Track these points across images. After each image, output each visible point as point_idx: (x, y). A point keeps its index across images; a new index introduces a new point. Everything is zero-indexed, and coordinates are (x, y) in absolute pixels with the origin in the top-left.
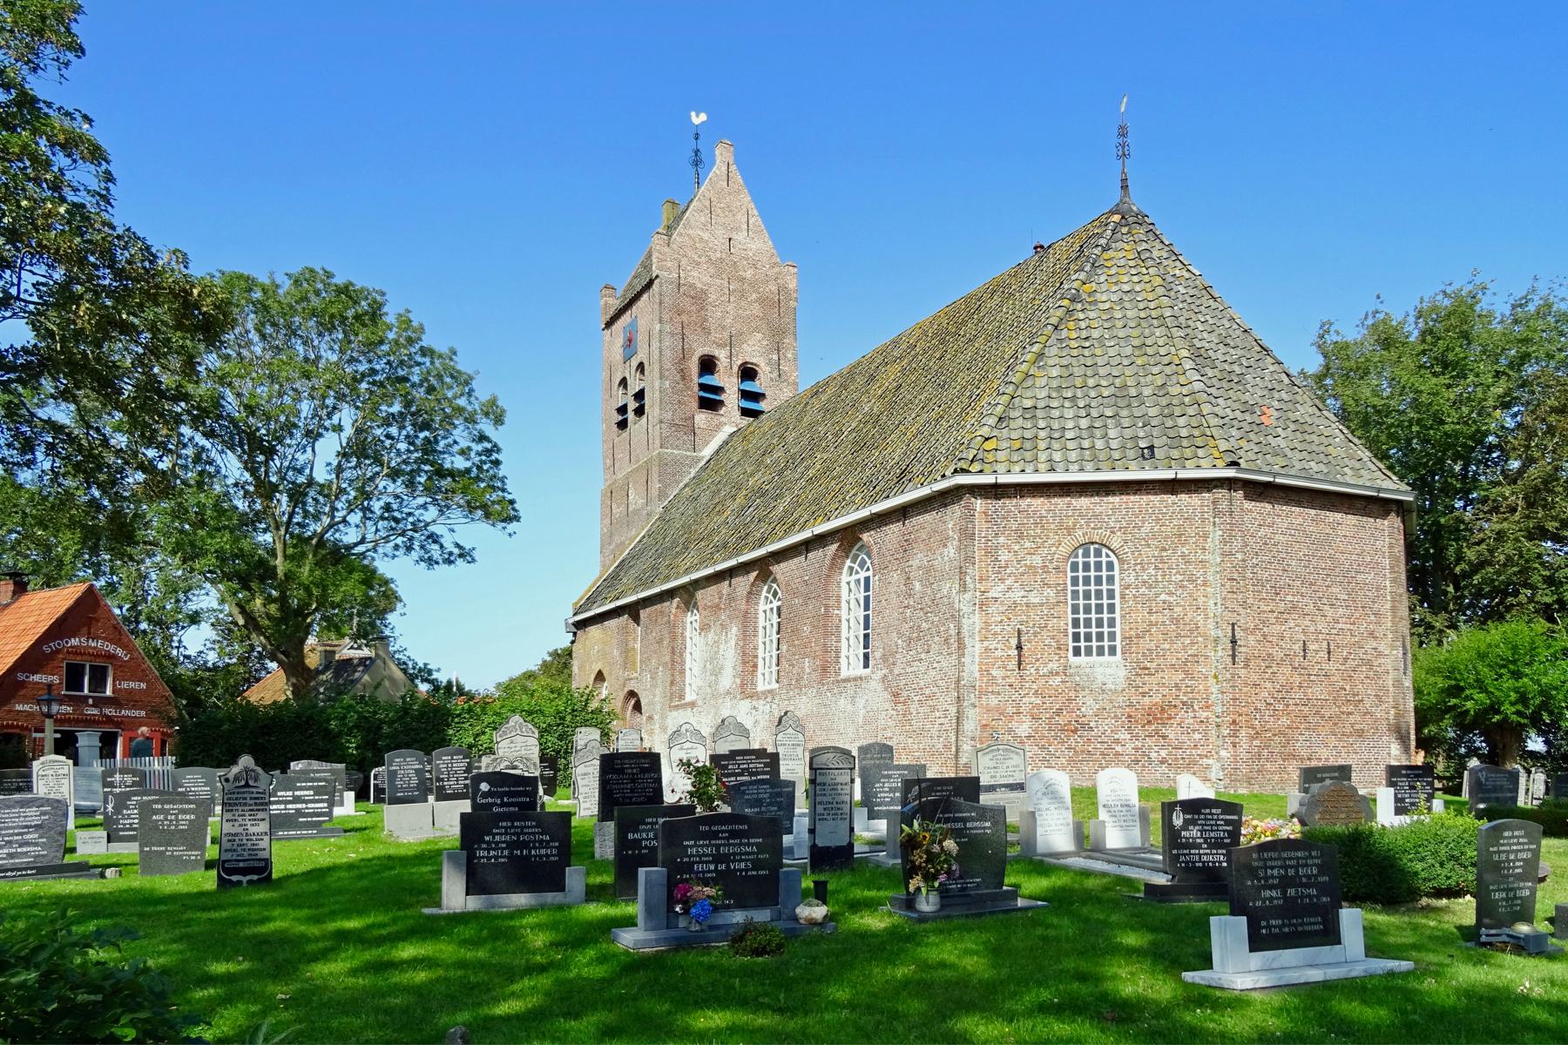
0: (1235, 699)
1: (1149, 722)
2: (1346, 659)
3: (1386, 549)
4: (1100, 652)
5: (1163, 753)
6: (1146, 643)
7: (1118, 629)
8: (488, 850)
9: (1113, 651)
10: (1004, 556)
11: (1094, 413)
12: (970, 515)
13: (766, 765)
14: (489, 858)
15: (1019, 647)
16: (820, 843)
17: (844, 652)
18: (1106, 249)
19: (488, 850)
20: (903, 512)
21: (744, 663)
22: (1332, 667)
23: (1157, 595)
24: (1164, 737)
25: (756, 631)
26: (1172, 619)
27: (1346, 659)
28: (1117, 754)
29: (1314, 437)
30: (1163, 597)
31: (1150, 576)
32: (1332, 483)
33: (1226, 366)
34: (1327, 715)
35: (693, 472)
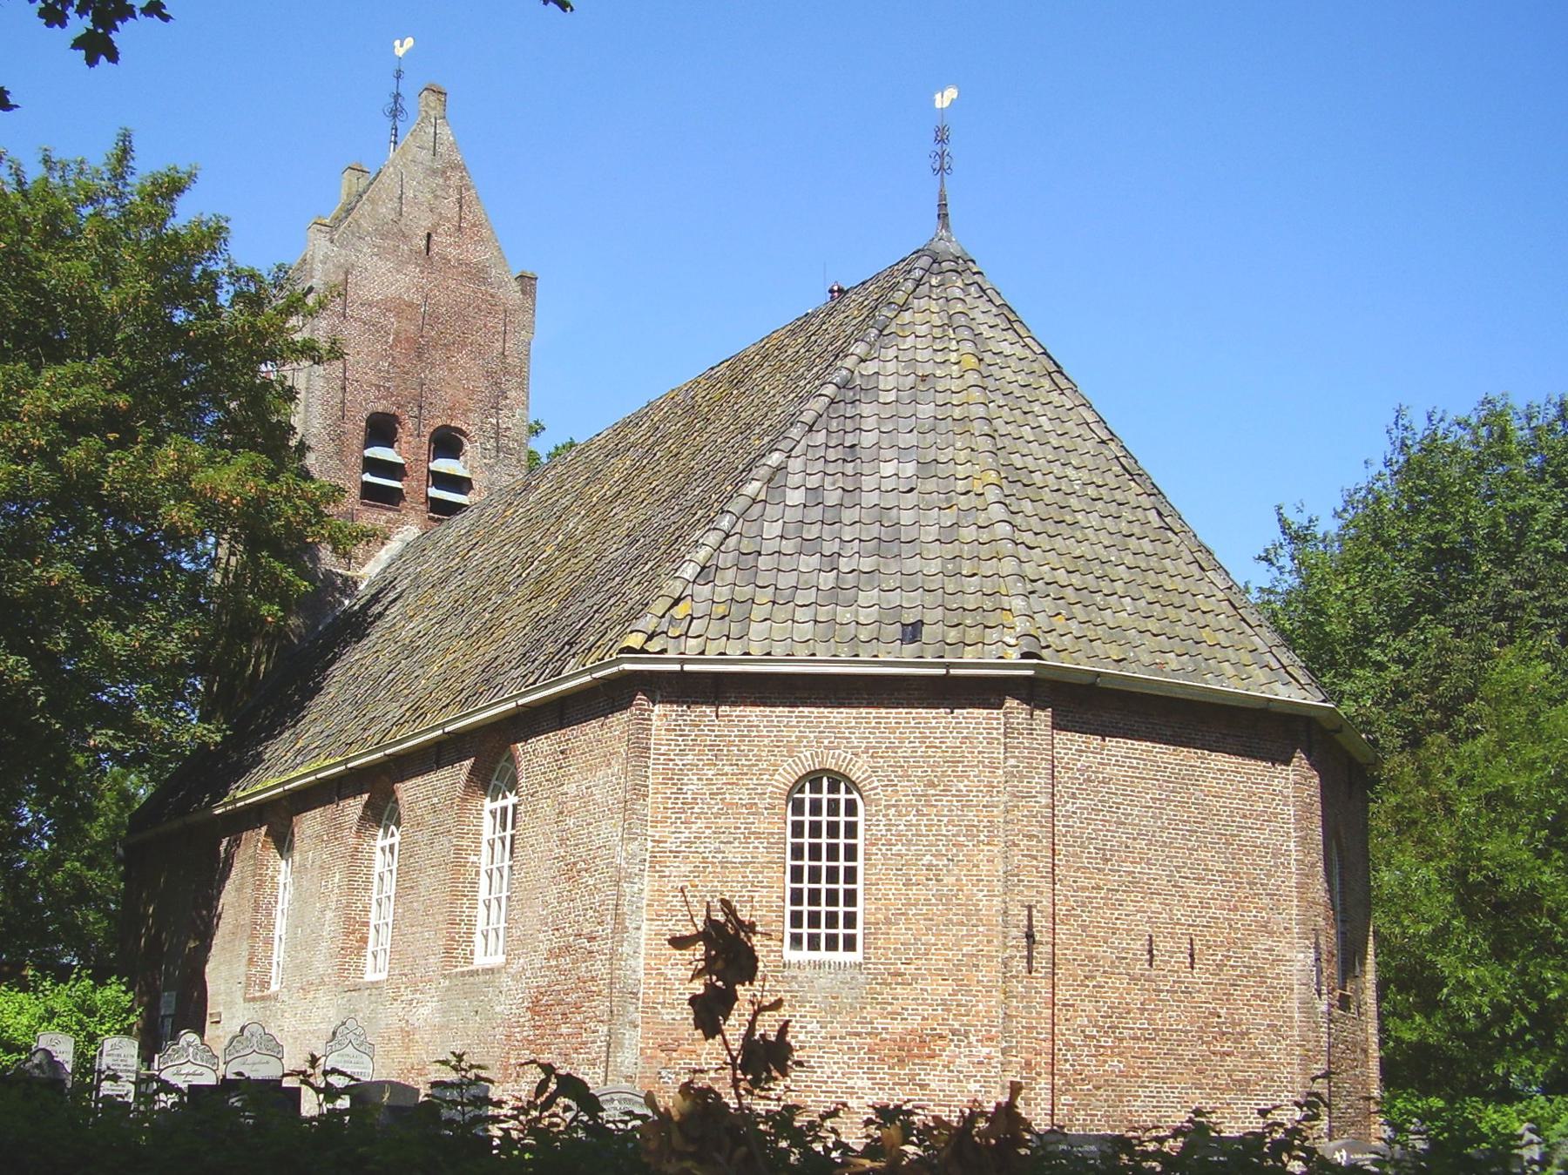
0: (1030, 1028)
1: (901, 1061)
2: (1220, 966)
3: (1289, 792)
4: (832, 944)
6: (900, 932)
7: (859, 909)
9: (850, 944)
10: (692, 785)
11: (844, 565)
12: (644, 722)
17: (481, 925)
18: (904, 307)
22: (1199, 976)
23: (919, 857)
25: (368, 881)
27: (1220, 966)
29: (1182, 614)
31: (909, 825)
33: (1058, 497)
34: (1188, 1055)
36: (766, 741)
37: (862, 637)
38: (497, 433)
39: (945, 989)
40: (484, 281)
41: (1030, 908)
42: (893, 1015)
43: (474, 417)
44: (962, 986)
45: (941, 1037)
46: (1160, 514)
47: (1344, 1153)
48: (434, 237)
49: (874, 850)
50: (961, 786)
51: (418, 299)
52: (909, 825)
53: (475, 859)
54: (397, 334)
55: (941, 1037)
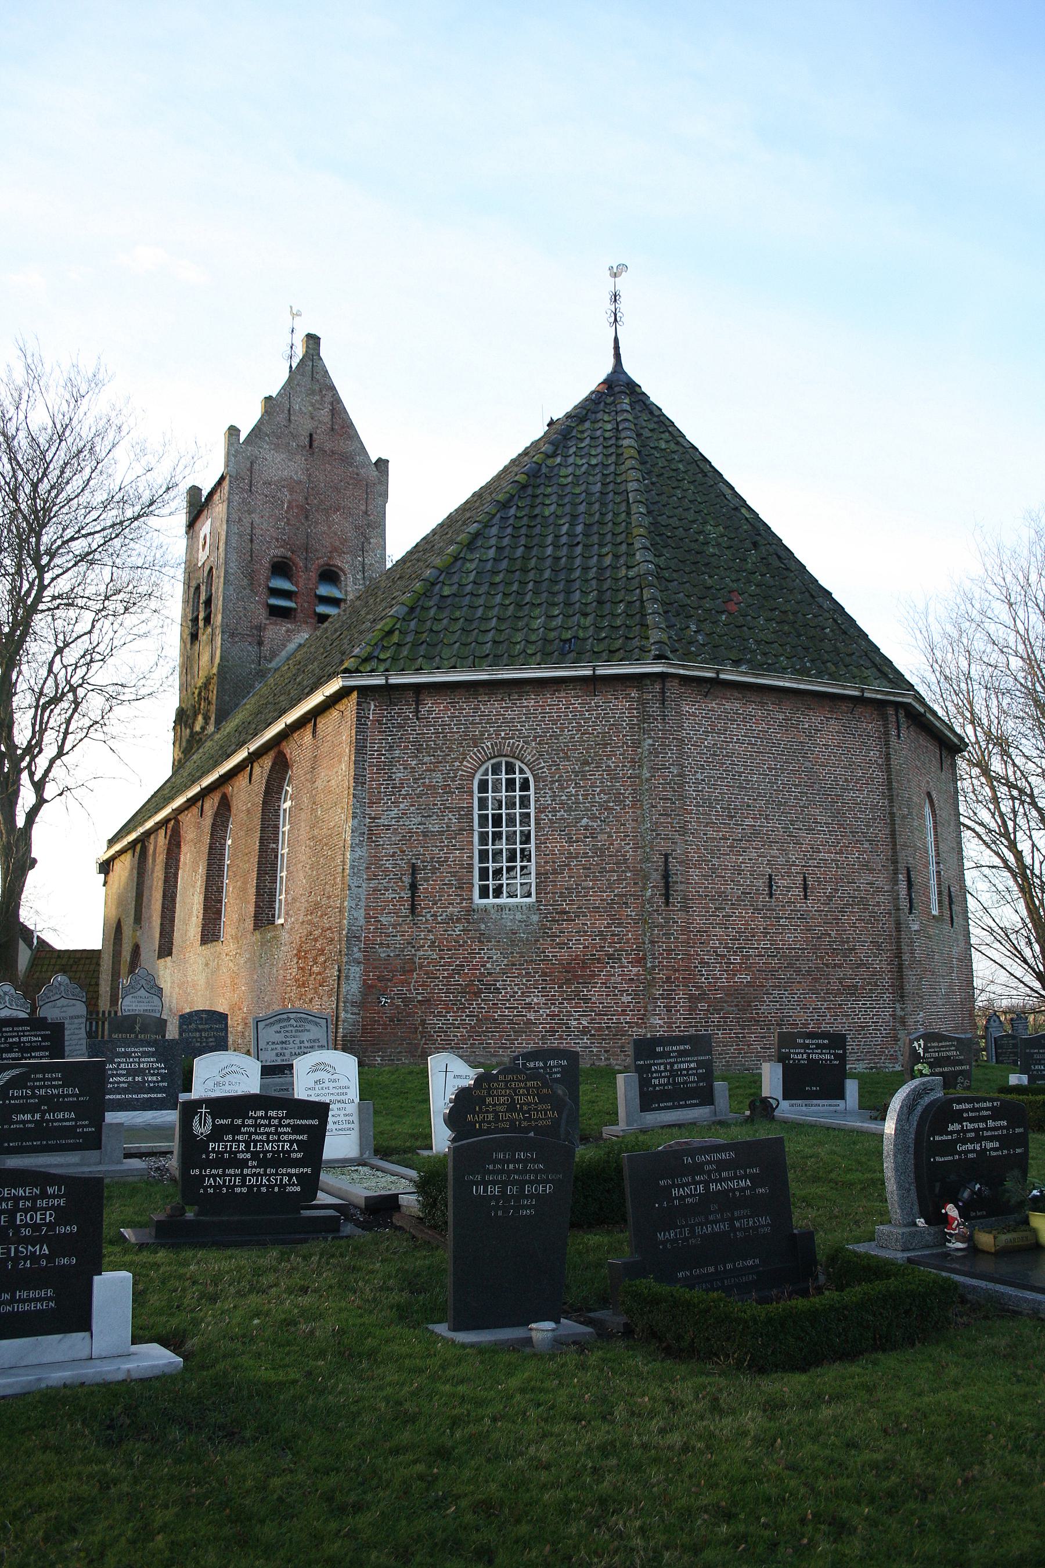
2: (830, 898)
6: (564, 880)
13: (45, 1038)
15: (413, 887)
24: (586, 1000)
27: (830, 898)
28: (529, 1022)
31: (569, 796)
36: (456, 736)
37: (529, 652)
38: (363, 568)
41: (666, 856)
46: (779, 557)
47: (922, 1042)
48: (314, 436)
49: (543, 816)
50: (610, 763)
51: (304, 478)
52: (569, 797)
53: (274, 846)
54: (289, 502)
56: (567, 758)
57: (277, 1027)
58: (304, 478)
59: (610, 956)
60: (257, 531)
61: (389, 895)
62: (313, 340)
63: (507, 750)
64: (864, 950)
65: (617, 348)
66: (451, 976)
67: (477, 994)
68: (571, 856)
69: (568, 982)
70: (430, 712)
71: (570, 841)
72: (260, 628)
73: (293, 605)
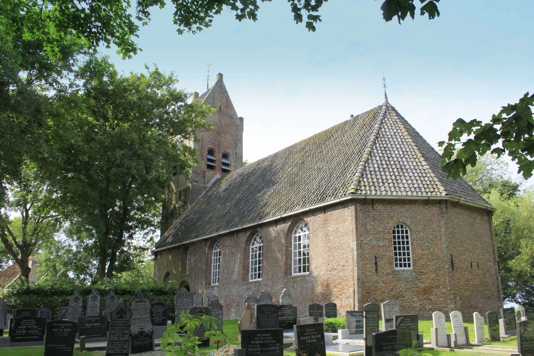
0: (454, 284)
4: (405, 266)
5: (430, 306)
6: (421, 262)
8: (253, 348)
9: (409, 266)
13: (292, 312)
14: (253, 352)
15: (376, 263)
16: (369, 345)
19: (253, 348)
20: (324, 209)
21: (244, 269)
23: (424, 243)
24: (430, 300)
26: (430, 253)
28: (414, 307)
30: (426, 244)
32: (474, 203)
35: (204, 192)
39: (433, 275)
40: (232, 118)
42: (422, 283)
43: (231, 150)
44: (437, 275)
45: (433, 287)
51: (218, 122)
55: (433, 287)
56: (420, 224)
57: (388, 307)
58: (218, 122)
59: (436, 286)
60: (204, 138)
61: (368, 266)
62: (221, 76)
63: (401, 221)
64: (490, 285)
65: (386, 95)
66: (389, 292)
67: (398, 298)
68: (423, 255)
69: (425, 294)
70: (377, 208)
71: (423, 250)
72: (204, 172)
73: (214, 165)
